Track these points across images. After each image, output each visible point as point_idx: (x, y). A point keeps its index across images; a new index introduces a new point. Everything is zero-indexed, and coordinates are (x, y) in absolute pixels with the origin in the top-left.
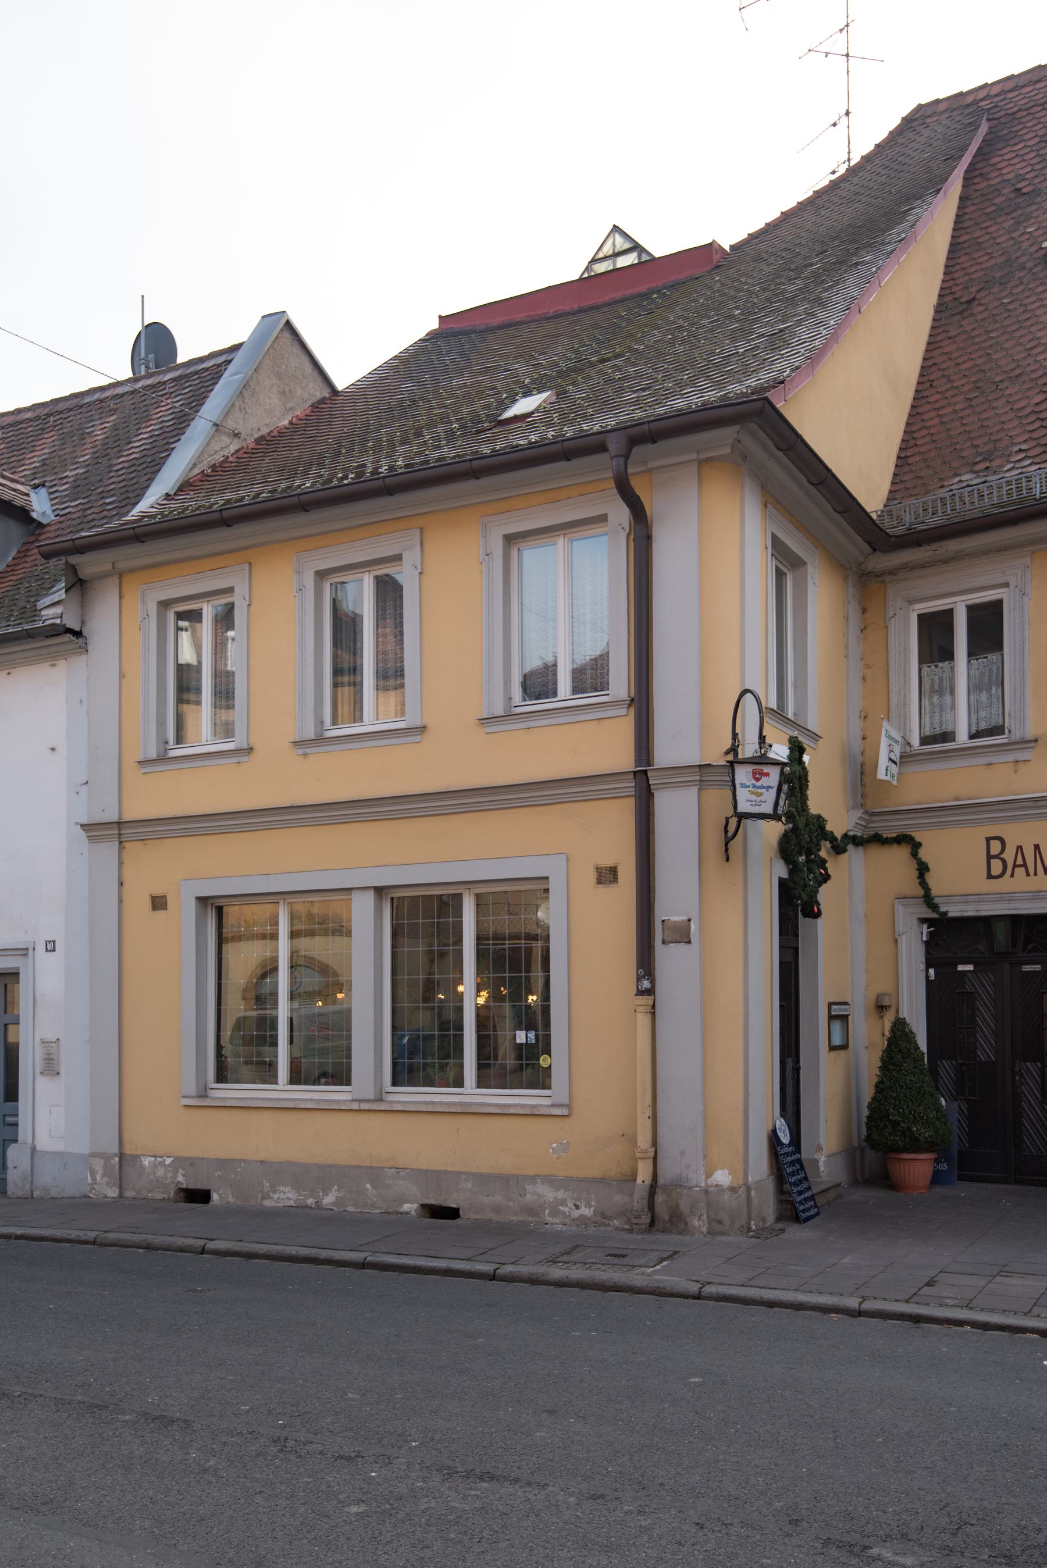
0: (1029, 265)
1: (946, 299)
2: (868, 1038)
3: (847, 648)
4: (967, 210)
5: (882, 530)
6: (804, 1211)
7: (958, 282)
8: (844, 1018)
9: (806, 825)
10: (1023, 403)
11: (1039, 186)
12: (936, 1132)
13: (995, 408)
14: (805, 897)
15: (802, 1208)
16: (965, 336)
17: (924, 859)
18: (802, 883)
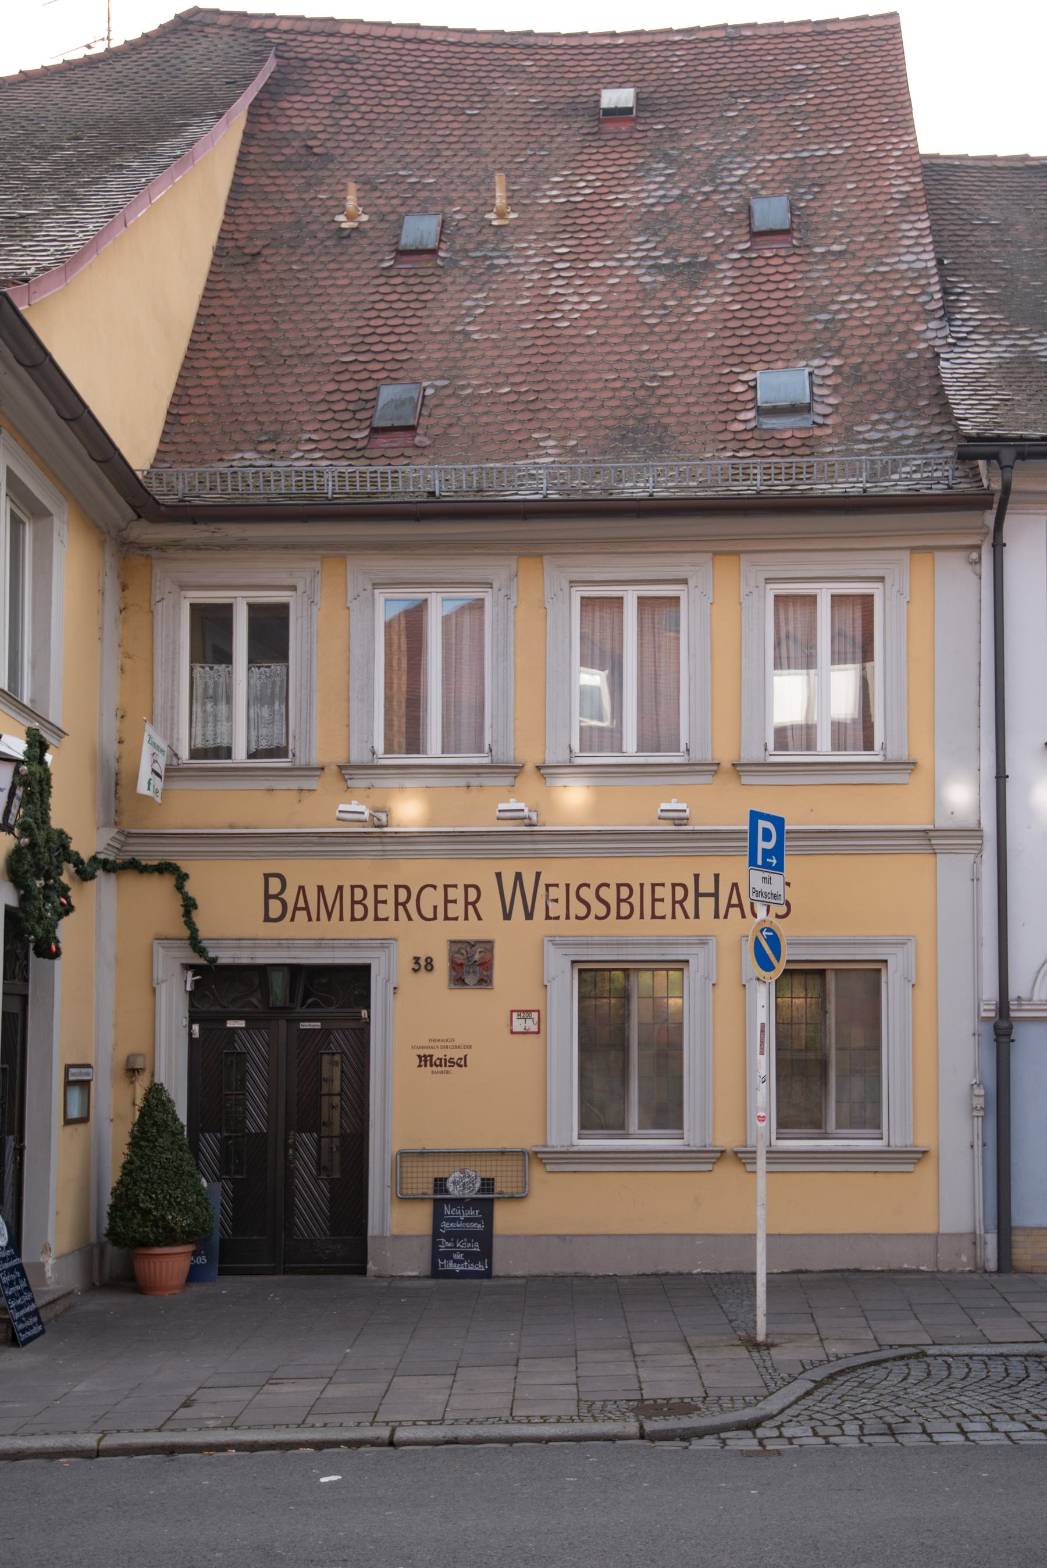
0: (321, 235)
1: (227, 244)
2: (115, 1109)
3: (101, 628)
4: (253, 150)
5: (150, 495)
6: (23, 1331)
7: (241, 228)
8: (85, 1085)
9: (47, 841)
10: (313, 388)
11: (332, 152)
12: (196, 1219)
13: (283, 385)
14: (40, 931)
15: (21, 1326)
16: (249, 294)
17: (191, 894)
18: (36, 913)
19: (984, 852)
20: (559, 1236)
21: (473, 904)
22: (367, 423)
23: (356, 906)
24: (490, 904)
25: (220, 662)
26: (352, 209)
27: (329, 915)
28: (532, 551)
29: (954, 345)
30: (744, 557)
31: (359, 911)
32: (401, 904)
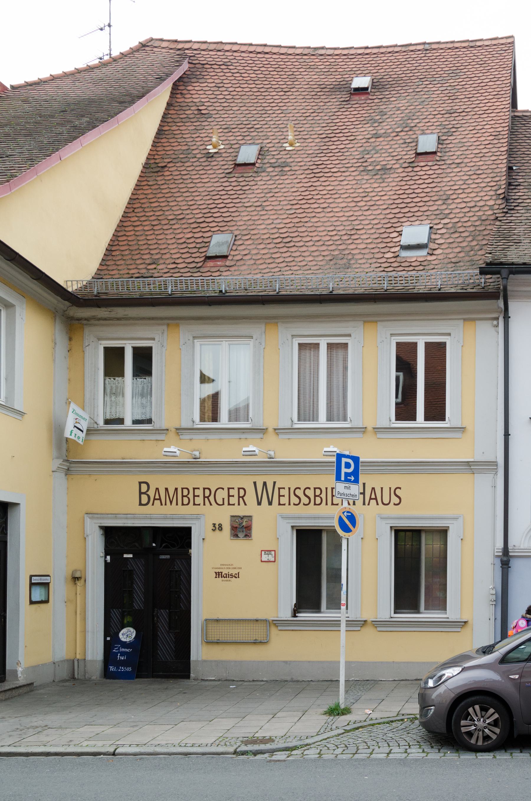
4: (171, 112)
19: (498, 473)
20: (284, 662)
21: (242, 497)
22: (204, 254)
23: (184, 498)
24: (251, 497)
25: (119, 376)
26: (215, 143)
27: (171, 502)
28: (271, 320)
29: (507, 213)
30: (379, 323)
31: (186, 500)
32: (206, 497)
